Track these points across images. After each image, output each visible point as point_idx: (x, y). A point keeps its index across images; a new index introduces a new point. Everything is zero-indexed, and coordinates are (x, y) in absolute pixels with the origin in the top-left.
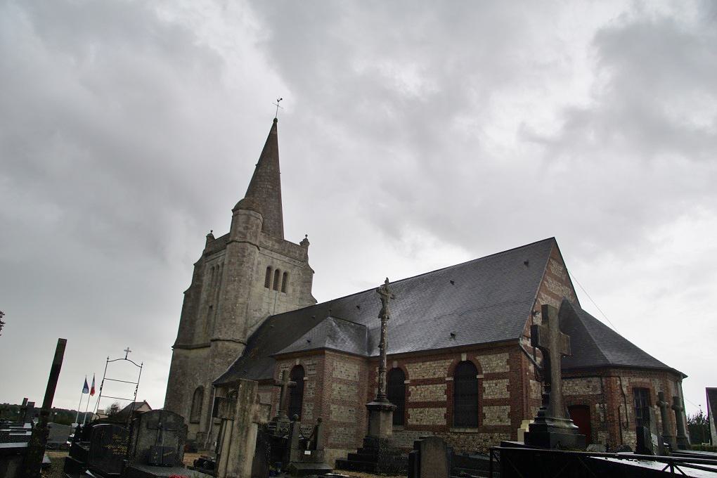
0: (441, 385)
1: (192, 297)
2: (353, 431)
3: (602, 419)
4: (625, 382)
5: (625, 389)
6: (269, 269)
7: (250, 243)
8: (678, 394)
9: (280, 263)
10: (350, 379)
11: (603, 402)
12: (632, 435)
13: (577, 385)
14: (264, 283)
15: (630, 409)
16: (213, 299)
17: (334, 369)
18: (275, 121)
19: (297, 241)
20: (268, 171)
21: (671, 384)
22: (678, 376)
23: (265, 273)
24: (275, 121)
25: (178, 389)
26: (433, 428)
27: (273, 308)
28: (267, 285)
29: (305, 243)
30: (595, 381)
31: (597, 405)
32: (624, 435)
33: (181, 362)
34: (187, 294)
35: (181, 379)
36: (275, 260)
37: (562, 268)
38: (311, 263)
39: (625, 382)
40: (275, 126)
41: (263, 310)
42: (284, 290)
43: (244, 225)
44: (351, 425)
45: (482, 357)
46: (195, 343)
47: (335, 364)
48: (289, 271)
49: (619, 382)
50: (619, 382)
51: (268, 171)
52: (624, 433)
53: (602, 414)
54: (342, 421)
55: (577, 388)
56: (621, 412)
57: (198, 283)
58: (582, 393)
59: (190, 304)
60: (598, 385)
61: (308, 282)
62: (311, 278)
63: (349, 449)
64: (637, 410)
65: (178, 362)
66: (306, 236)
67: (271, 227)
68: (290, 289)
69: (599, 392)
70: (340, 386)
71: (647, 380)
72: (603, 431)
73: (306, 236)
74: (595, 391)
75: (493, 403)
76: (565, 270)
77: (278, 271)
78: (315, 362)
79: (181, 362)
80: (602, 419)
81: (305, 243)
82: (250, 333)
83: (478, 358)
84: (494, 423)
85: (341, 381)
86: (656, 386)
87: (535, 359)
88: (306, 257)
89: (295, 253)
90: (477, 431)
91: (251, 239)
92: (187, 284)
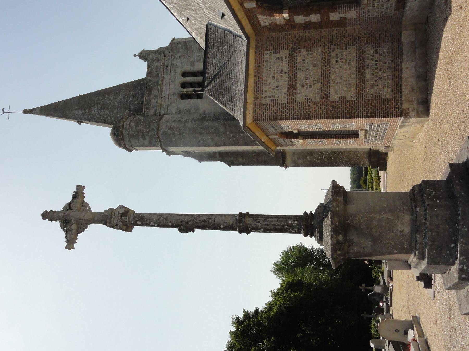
1: (232, 159)
2: (370, 50)
6: (183, 96)
7: (158, 129)
9: (172, 84)
10: (286, 69)
18: (26, 112)
19: (144, 65)
24: (26, 112)
25: (327, 158)
29: (144, 55)
33: (299, 158)
34: (231, 163)
35: (316, 156)
36: (171, 92)
38: (165, 43)
40: (31, 111)
43: (141, 139)
44: (361, 58)
47: (267, 101)
48: (179, 71)
54: (354, 76)
59: (241, 160)
61: (186, 46)
63: (400, 54)
65: (300, 161)
66: (135, 56)
67: (137, 100)
70: (298, 87)
73: (135, 56)
79: (299, 158)
81: (144, 55)
85: (292, 86)
89: (157, 67)
91: (153, 130)
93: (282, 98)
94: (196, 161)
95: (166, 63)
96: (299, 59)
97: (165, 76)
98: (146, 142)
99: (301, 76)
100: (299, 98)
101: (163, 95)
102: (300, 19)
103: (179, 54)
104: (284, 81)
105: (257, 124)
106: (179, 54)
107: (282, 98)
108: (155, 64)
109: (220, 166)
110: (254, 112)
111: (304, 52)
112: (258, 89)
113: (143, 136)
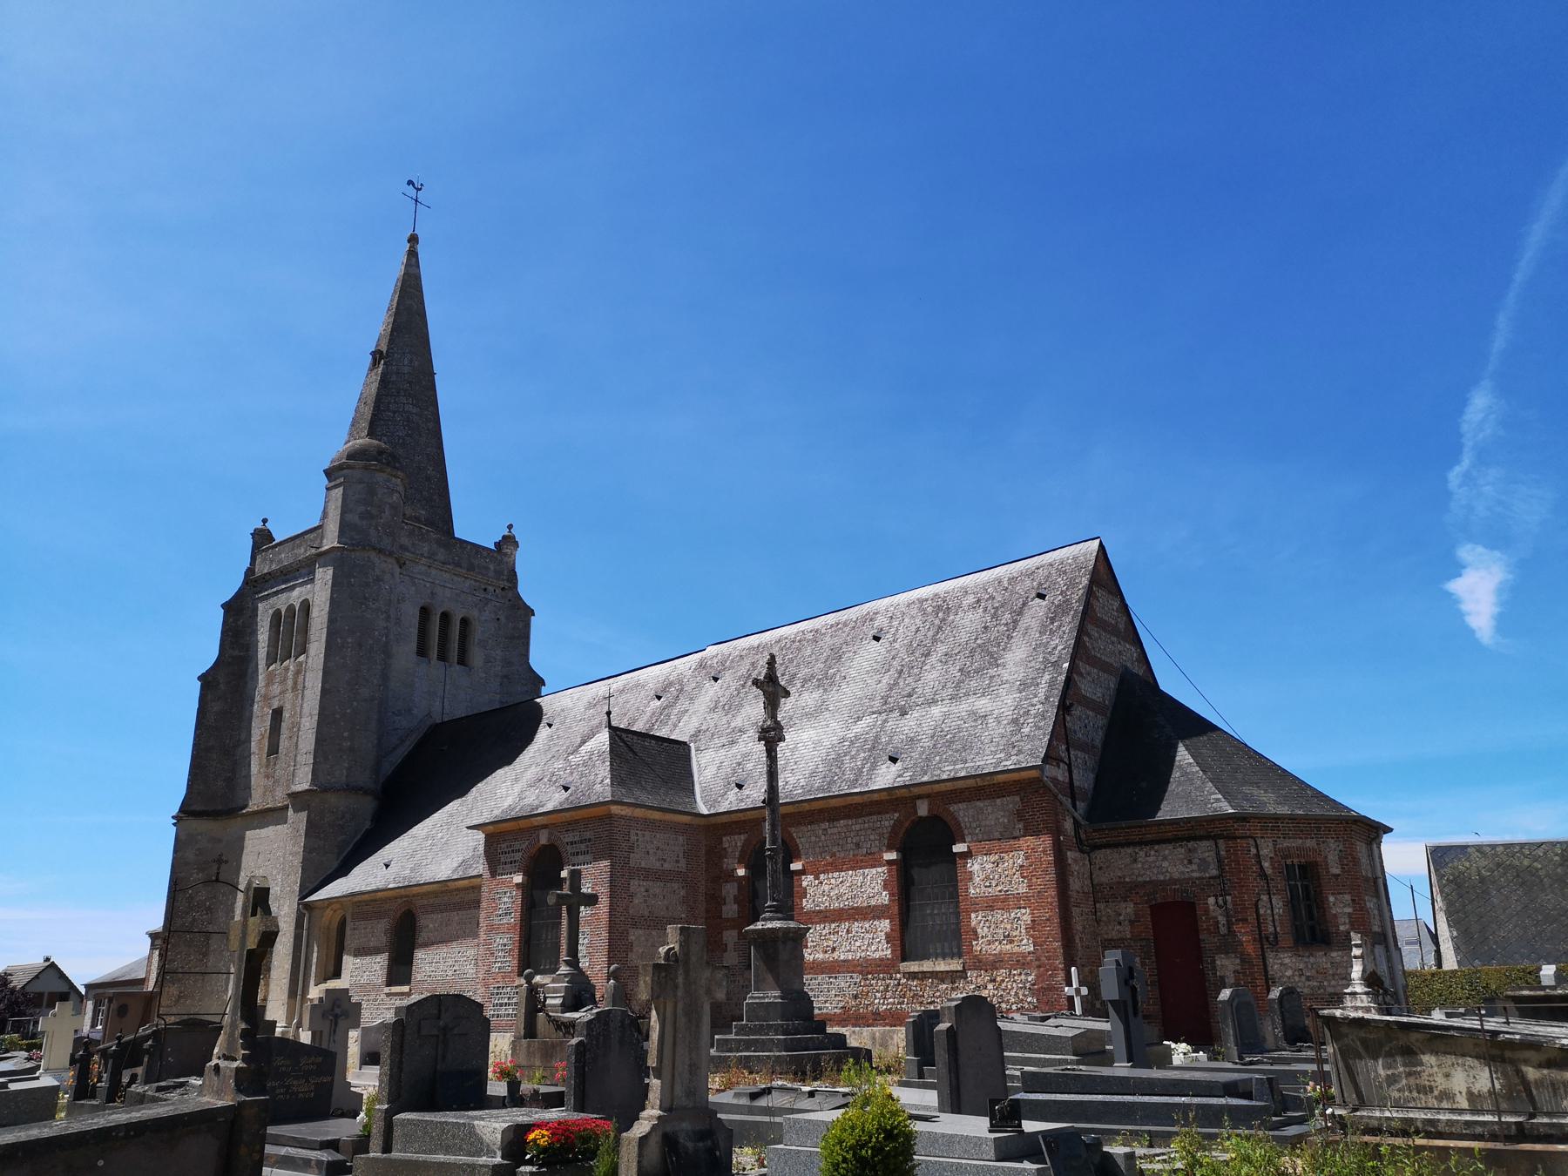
0: (874, 871)
3: (1223, 930)
4: (1266, 850)
5: (1266, 865)
6: (425, 612)
7: (380, 551)
8: (1374, 871)
9: (452, 593)
10: (666, 866)
11: (1224, 893)
12: (1287, 961)
13: (1165, 858)
14: (414, 646)
15: (1278, 902)
16: (283, 692)
17: (631, 848)
18: (413, 239)
20: (406, 369)
21: (1361, 848)
22: (1374, 831)
23: (416, 621)
24: (413, 239)
26: (867, 968)
27: (438, 703)
28: (422, 651)
29: (509, 541)
30: (1205, 850)
31: (1211, 900)
32: (1270, 961)
37: (1116, 604)
38: (526, 591)
39: (1266, 850)
40: (413, 254)
41: (415, 711)
42: (462, 661)
43: (362, 508)
45: (962, 806)
46: (1012, 802)
47: (633, 838)
48: (474, 613)
49: (1253, 851)
50: (1253, 851)
51: (406, 369)
52: (1270, 957)
53: (1222, 920)
55: (1165, 864)
56: (1262, 911)
57: (236, 653)
58: (1176, 876)
59: (216, 707)
60: (1210, 856)
62: (528, 626)
64: (1292, 904)
66: (510, 527)
68: (477, 657)
69: (1215, 872)
71: (1310, 843)
72: (1227, 953)
73: (510, 527)
74: (1205, 871)
75: (991, 904)
76: (1125, 607)
77: (445, 617)
78: (588, 835)
80: (1223, 930)
81: (509, 541)
82: (388, 768)
83: (1161, 816)
84: (996, 948)
86: (1331, 855)
87: (1074, 806)
88: (512, 577)
89: (487, 568)
90: (955, 965)
92: (209, 654)
93: (637, 859)
94: (228, 595)
95: (491, 589)
96: (676, 886)
97: (468, 583)
98: (353, 518)
99: (656, 888)
100: (634, 883)
101: (434, 572)
102: (730, 890)
103: (503, 620)
104: (652, 862)
105: (600, 818)
106: (503, 620)
107: (637, 859)
108: (492, 567)
109: (207, 651)
110: (622, 817)
111: (683, 893)
112: (649, 825)
113: (366, 516)
